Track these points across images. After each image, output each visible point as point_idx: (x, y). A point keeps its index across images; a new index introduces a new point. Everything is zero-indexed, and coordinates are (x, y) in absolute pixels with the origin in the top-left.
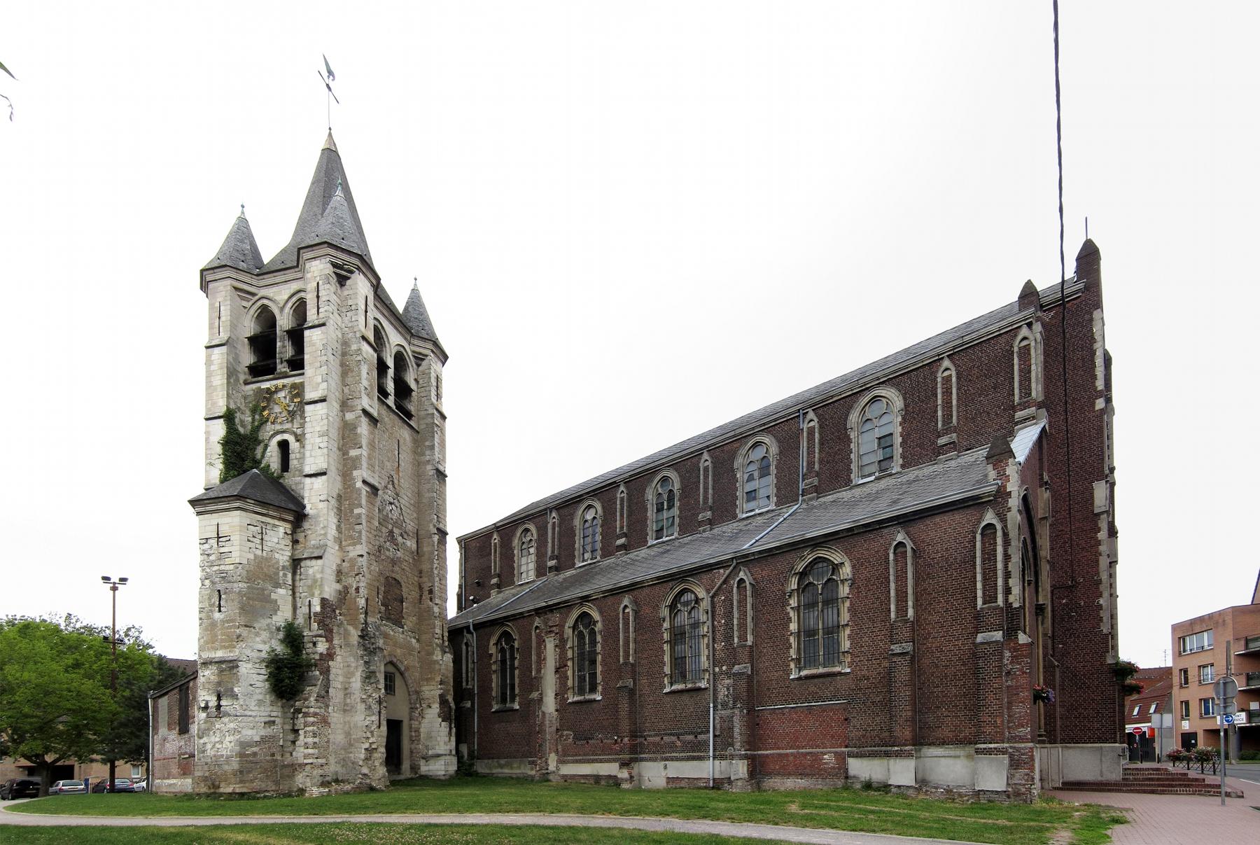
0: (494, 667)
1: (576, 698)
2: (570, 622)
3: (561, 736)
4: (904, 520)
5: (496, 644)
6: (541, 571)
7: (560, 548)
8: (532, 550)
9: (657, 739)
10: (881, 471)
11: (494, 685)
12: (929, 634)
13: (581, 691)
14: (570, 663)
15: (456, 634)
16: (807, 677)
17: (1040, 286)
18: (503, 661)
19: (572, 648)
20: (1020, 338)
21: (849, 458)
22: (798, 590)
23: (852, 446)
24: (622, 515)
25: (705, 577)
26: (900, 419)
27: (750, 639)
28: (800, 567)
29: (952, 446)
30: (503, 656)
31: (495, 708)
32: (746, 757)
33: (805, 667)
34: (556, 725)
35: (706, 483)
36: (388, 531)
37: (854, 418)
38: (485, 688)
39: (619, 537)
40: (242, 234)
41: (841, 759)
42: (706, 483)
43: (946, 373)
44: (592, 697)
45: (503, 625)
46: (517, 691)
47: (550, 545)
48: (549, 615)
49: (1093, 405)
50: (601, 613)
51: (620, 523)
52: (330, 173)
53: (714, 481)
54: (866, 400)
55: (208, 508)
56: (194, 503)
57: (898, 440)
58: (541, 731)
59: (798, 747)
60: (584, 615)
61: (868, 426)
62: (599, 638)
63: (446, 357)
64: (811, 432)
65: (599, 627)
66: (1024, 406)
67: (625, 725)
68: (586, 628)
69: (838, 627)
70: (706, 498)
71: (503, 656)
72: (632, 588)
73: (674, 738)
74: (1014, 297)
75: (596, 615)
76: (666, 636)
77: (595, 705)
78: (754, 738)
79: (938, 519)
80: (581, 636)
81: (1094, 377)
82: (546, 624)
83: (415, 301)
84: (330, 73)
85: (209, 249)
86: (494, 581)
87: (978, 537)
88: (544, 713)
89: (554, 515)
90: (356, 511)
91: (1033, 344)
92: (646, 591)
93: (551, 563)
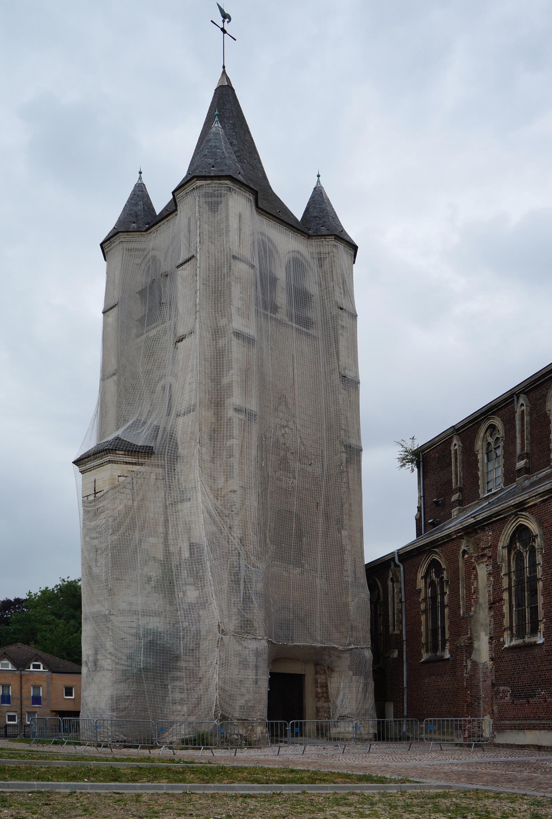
0: (423, 606)
1: (514, 643)
3: (498, 692)
5: (425, 577)
6: (510, 475)
7: (531, 443)
8: (500, 452)
11: (423, 629)
13: (521, 634)
14: (506, 596)
15: (379, 570)
18: (434, 598)
19: (425, 600)
31: (425, 656)
34: (491, 678)
36: (276, 457)
38: (414, 633)
40: (140, 195)
44: (533, 640)
45: (431, 552)
46: (447, 636)
47: (518, 441)
48: (481, 535)
50: (540, 523)
55: (88, 466)
60: (522, 530)
62: (539, 559)
63: (355, 248)
68: (525, 545)
71: (434, 592)
75: (534, 527)
80: (519, 557)
83: (318, 201)
84: (225, 16)
85: (109, 218)
86: (455, 497)
88: (475, 664)
89: (521, 401)
90: (229, 443)
93: (520, 464)
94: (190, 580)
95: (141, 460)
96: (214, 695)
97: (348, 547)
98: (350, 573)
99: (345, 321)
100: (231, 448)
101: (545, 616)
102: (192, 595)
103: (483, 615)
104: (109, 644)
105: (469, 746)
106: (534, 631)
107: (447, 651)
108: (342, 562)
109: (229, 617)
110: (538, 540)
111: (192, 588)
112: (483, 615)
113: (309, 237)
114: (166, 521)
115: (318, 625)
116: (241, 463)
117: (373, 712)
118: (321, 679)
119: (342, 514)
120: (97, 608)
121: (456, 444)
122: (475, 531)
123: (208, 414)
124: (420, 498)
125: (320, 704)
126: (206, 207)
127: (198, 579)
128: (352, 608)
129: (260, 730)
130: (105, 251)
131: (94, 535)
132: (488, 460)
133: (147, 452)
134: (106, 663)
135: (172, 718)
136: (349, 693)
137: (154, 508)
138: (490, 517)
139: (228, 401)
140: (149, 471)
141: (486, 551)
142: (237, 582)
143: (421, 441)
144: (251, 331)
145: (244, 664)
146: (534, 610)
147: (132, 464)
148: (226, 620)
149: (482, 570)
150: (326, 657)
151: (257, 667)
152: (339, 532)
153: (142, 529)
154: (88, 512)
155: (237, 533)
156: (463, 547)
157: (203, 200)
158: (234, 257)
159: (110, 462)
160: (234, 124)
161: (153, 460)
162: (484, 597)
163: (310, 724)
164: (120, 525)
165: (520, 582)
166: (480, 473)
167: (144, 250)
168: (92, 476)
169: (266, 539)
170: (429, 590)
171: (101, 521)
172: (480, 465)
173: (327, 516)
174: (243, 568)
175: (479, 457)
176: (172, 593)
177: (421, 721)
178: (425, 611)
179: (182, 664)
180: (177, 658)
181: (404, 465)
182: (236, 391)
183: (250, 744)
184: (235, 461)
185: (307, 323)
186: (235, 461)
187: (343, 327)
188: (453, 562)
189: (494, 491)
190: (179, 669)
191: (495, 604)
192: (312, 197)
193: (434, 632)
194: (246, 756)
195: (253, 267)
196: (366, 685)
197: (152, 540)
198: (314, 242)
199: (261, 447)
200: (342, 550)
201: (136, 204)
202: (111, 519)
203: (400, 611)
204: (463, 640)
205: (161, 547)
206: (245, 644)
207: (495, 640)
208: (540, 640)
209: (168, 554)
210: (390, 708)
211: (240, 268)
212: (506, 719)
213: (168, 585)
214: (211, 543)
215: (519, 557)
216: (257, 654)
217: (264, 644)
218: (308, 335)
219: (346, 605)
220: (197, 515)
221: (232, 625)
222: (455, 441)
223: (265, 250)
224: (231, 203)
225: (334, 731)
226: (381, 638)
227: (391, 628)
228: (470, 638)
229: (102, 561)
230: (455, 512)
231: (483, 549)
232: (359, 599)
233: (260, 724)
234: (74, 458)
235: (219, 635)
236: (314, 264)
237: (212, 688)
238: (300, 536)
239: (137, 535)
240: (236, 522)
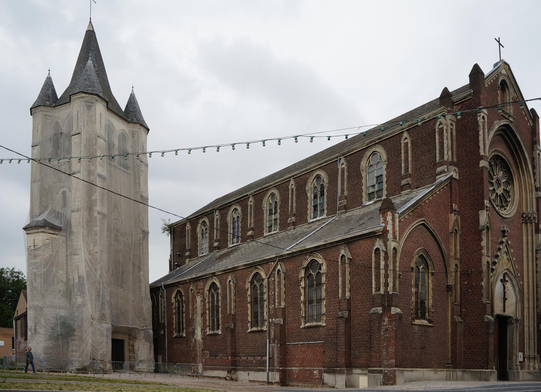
0: (174, 311)
1: (211, 332)
2: (207, 288)
4: (348, 242)
5: (175, 297)
6: (212, 249)
8: (207, 235)
9: (245, 358)
10: (378, 197)
11: (174, 322)
12: (357, 306)
13: (213, 329)
14: (207, 312)
16: (309, 327)
17: (451, 90)
18: (179, 308)
19: (175, 308)
20: (403, 138)
21: (361, 189)
22: (305, 277)
23: (363, 181)
24: (251, 216)
25: (265, 266)
26: (385, 166)
27: (348, 294)
28: (305, 264)
29: (408, 186)
30: (179, 305)
31: (175, 335)
32: (278, 370)
33: (308, 322)
35: (292, 199)
37: (364, 164)
38: (170, 323)
39: (249, 230)
40: (49, 85)
41: (321, 372)
42: (292, 199)
43: (406, 141)
44: (216, 332)
46: (184, 326)
48: (198, 283)
49: (479, 164)
51: (251, 221)
52: (90, 45)
53: (297, 197)
54: (370, 153)
55: (30, 232)
56: (25, 229)
57: (385, 179)
58: (194, 350)
59: (304, 366)
60: (213, 284)
61: (372, 169)
62: (220, 298)
63: (148, 130)
64: (343, 169)
65: (324, 268)
66: (441, 164)
67: (229, 350)
68: (215, 291)
69: (319, 301)
70: (292, 211)
71: (179, 305)
72: (234, 270)
73: (252, 358)
74: (438, 95)
76: (249, 299)
77: (219, 337)
78: (284, 360)
79: (361, 242)
81: (479, 147)
82: (197, 289)
83: (132, 101)
85: (34, 94)
86: (187, 254)
87: (373, 255)
88: (195, 340)
89: (217, 213)
90: (95, 229)
91: (445, 128)
92: (241, 272)
94: (79, 293)
95: (56, 233)
96: (90, 348)
97: (143, 280)
98: (144, 293)
99: (143, 168)
100: (96, 231)
101: (222, 323)
102: (79, 300)
103: (199, 319)
104: (42, 321)
105: (193, 376)
106: (218, 328)
107: (184, 333)
108: (140, 287)
109: (95, 312)
110: (220, 290)
111: (80, 297)
112: (199, 319)
113: (129, 122)
114: (67, 263)
115: (130, 316)
116: (100, 239)
117: (153, 359)
118: (131, 342)
119: (140, 264)
120: (36, 303)
121: (188, 227)
122: (196, 281)
123: (86, 213)
124: (171, 250)
125: (131, 354)
126: (86, 107)
127: (82, 293)
128: (145, 309)
129: (109, 366)
130: (32, 113)
131: (34, 267)
132: (202, 238)
133: (59, 229)
134: (41, 331)
135: (72, 359)
136: (143, 350)
137: (62, 256)
138: (202, 276)
139: (95, 208)
140: (59, 238)
141: (200, 291)
142: (99, 296)
143: (174, 220)
144: (104, 174)
145: (102, 335)
146: (218, 319)
147: (52, 234)
148: (94, 313)
149: (199, 299)
150: (133, 332)
151: (107, 336)
152: (139, 272)
153: (57, 266)
154: (31, 255)
155: (98, 272)
156: (191, 288)
157: (84, 103)
158: (98, 136)
159: (42, 232)
160: (95, 54)
161: (62, 233)
162: (199, 311)
163: (126, 363)
164: (47, 264)
165: (213, 306)
166: (198, 244)
167: (53, 116)
168: (32, 237)
169: (214, 383)
170: (177, 304)
171: (38, 260)
172: (198, 240)
173: (134, 265)
174: (101, 289)
175: (198, 236)
176: (70, 298)
177: (175, 364)
178: (175, 313)
179: (76, 333)
180: (74, 330)
181: (164, 232)
182: (98, 203)
183: (105, 372)
184: (98, 238)
185: (126, 167)
186: (98, 238)
187: (142, 171)
188: (187, 292)
189: (204, 254)
190: (75, 336)
191: (203, 314)
192: (130, 99)
193: (179, 323)
194: (106, 376)
195: (106, 141)
196: (150, 346)
197: (61, 272)
198: (131, 125)
199: (109, 230)
200: (140, 281)
201: (48, 90)
202: (43, 261)
203: (164, 312)
204: (191, 329)
205: (65, 276)
206: (102, 325)
207: (203, 330)
208: (220, 332)
209: (68, 279)
210: (160, 358)
211: (101, 142)
212: (207, 365)
213: (68, 294)
214: (87, 276)
215: (213, 295)
216: (107, 330)
217: (109, 326)
218: (127, 173)
219: (142, 308)
220: (81, 262)
221: (97, 316)
222: (188, 225)
223: (110, 129)
224: (97, 108)
225: (137, 367)
226: (157, 325)
227: (160, 320)
228: (194, 329)
229: (38, 280)
230: (187, 261)
231: (199, 289)
232: (147, 305)
233: (109, 363)
234: (24, 225)
235: (92, 321)
236: (130, 137)
237: (89, 345)
238: (123, 273)
239: (54, 269)
240: (98, 267)
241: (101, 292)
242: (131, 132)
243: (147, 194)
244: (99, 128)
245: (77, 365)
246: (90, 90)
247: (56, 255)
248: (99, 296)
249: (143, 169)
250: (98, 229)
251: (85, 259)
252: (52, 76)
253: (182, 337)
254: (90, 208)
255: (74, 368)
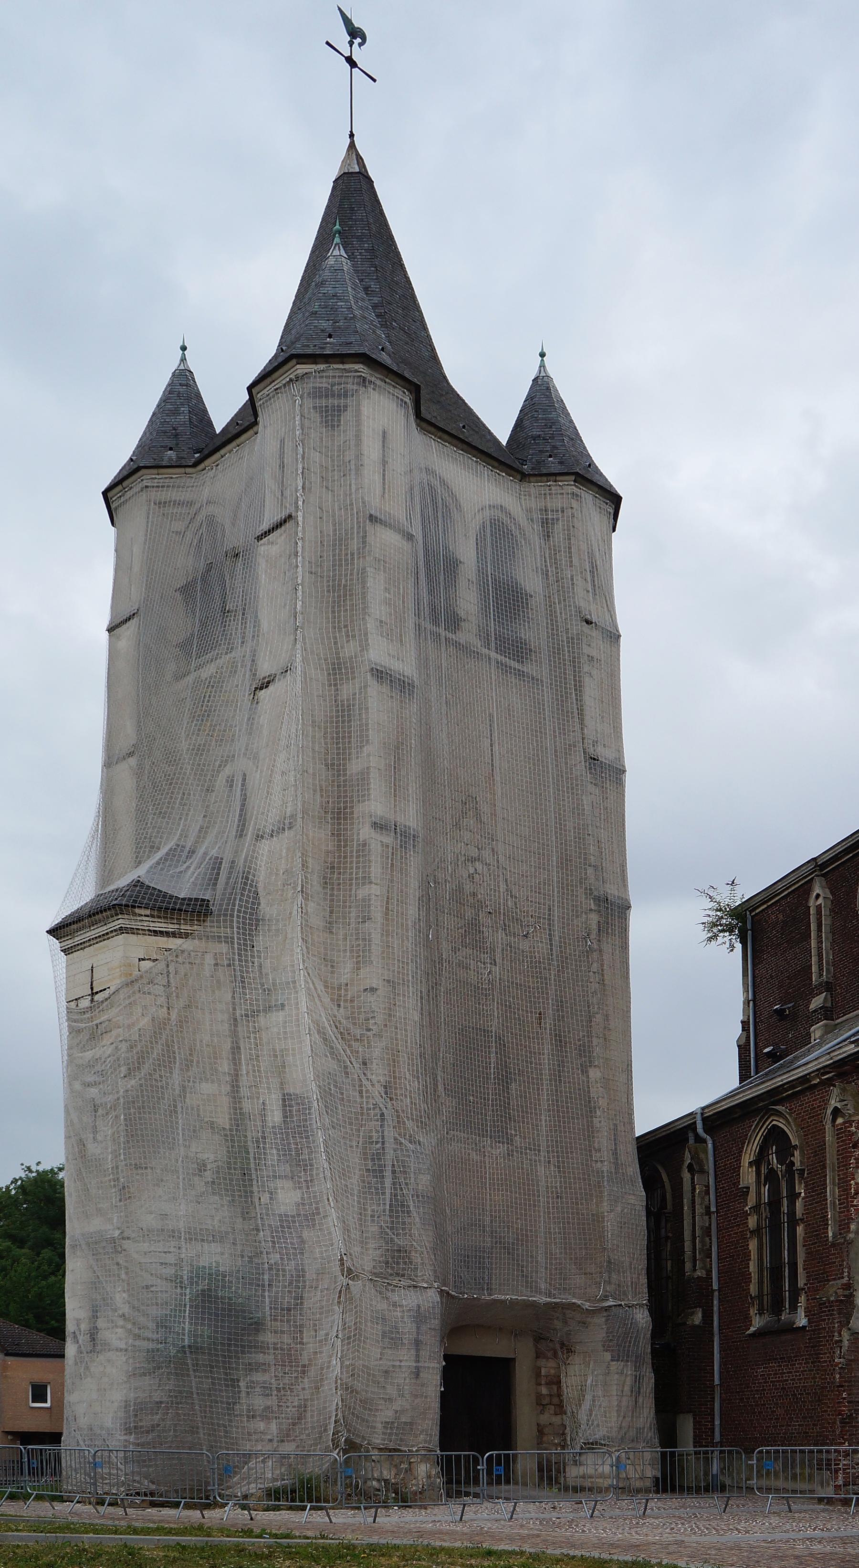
0: (752, 1222)
5: (756, 1163)
11: (753, 1267)
15: (663, 1149)
19: (756, 1208)
31: (757, 1323)
36: (456, 921)
38: (735, 1276)
40: (182, 393)
45: (768, 1112)
46: (801, 1283)
52: (354, 209)
55: (77, 939)
63: (615, 500)
71: (775, 1192)
83: (542, 407)
84: (355, 33)
86: (817, 1002)
90: (362, 893)
94: (284, 1169)
96: (335, 1400)
99: (596, 646)
102: (287, 1198)
104: (120, 1298)
108: (590, 1131)
109: (363, 1243)
111: (289, 1184)
113: (524, 477)
114: (236, 1049)
116: (385, 933)
117: (651, 1434)
118: (547, 1367)
120: (96, 1224)
123: (320, 835)
124: (747, 1003)
125: (545, 1418)
126: (316, 417)
127: (300, 1166)
128: (610, 1224)
129: (423, 1470)
130: (113, 506)
131: (90, 1078)
133: (196, 910)
134: (115, 1336)
135: (247, 1447)
136: (605, 1396)
137: (211, 1025)
139: (360, 809)
140: (201, 949)
144: (406, 666)
145: (392, 1338)
148: (357, 1249)
150: (558, 1324)
151: (418, 1343)
152: (585, 1071)
153: (188, 1065)
154: (79, 1031)
155: (378, 1073)
156: (834, 1103)
157: (309, 403)
158: (372, 518)
159: (122, 930)
160: (372, 251)
161: (210, 927)
163: (525, 1458)
167: (191, 503)
168: (86, 958)
171: (104, 1049)
173: (559, 1041)
174: (390, 1145)
177: (749, 1452)
179: (268, 1338)
180: (258, 1326)
182: (377, 787)
183: (404, 1499)
185: (518, 650)
186: (374, 929)
187: (591, 659)
190: (262, 1348)
192: (530, 398)
195: (410, 537)
196: (638, 1380)
197: (207, 1088)
198: (533, 488)
199: (427, 900)
201: (175, 412)
202: (124, 1047)
203: (707, 1231)
205: (225, 1101)
206: (395, 1297)
209: (239, 1117)
210: (686, 1427)
213: (238, 1178)
214: (325, 1093)
216: (419, 1317)
217: (433, 1296)
218: (521, 674)
219: (598, 1219)
220: (297, 1038)
221: (368, 1259)
222: (817, 890)
223: (436, 505)
225: (573, 1473)
227: (688, 1266)
229: (106, 1130)
230: (816, 1031)
232: (624, 1206)
233: (425, 1459)
236: (533, 532)
237: (328, 1387)
239: (176, 1078)
240: (377, 1052)
241: (390, 1154)
242: (536, 516)
243: (620, 750)
244: (378, 491)
245: (268, 1473)
246: (331, 346)
247: (181, 1023)
248: (379, 1173)
249: (594, 653)
250: (375, 890)
251: (317, 1023)
252: (192, 365)
253: (791, 1329)
254: (338, 813)
255: (253, 1488)
